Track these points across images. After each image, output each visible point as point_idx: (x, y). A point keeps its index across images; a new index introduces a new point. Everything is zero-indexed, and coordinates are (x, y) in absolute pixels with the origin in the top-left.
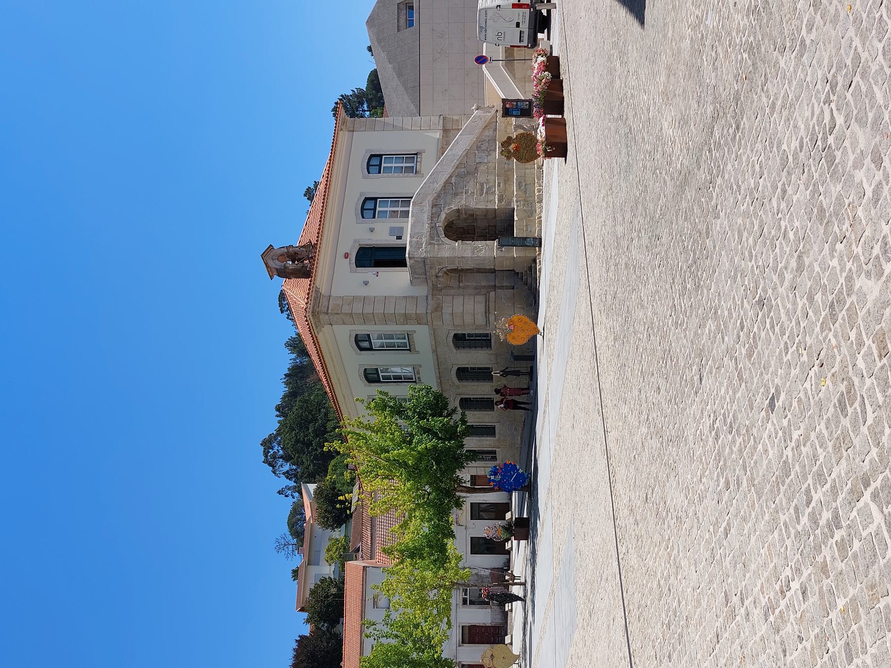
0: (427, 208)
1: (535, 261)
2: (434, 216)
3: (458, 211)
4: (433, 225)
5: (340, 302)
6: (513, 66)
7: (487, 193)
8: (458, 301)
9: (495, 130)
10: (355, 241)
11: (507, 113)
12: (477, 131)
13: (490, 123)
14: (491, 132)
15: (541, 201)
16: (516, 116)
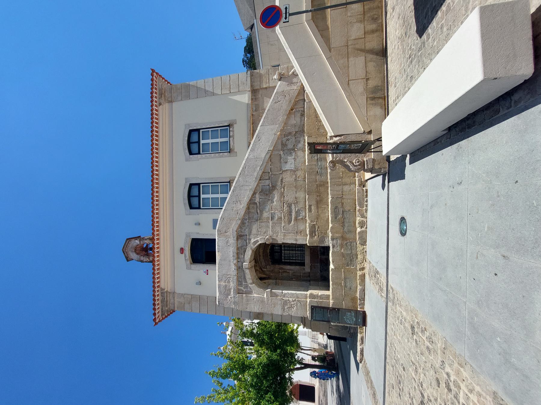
0: (232, 241)
2: (240, 252)
4: (240, 264)
5: (182, 300)
6: (325, 18)
7: (296, 219)
9: (303, 115)
10: (187, 235)
12: (281, 118)
13: (296, 103)
14: (298, 119)
15: (364, 242)
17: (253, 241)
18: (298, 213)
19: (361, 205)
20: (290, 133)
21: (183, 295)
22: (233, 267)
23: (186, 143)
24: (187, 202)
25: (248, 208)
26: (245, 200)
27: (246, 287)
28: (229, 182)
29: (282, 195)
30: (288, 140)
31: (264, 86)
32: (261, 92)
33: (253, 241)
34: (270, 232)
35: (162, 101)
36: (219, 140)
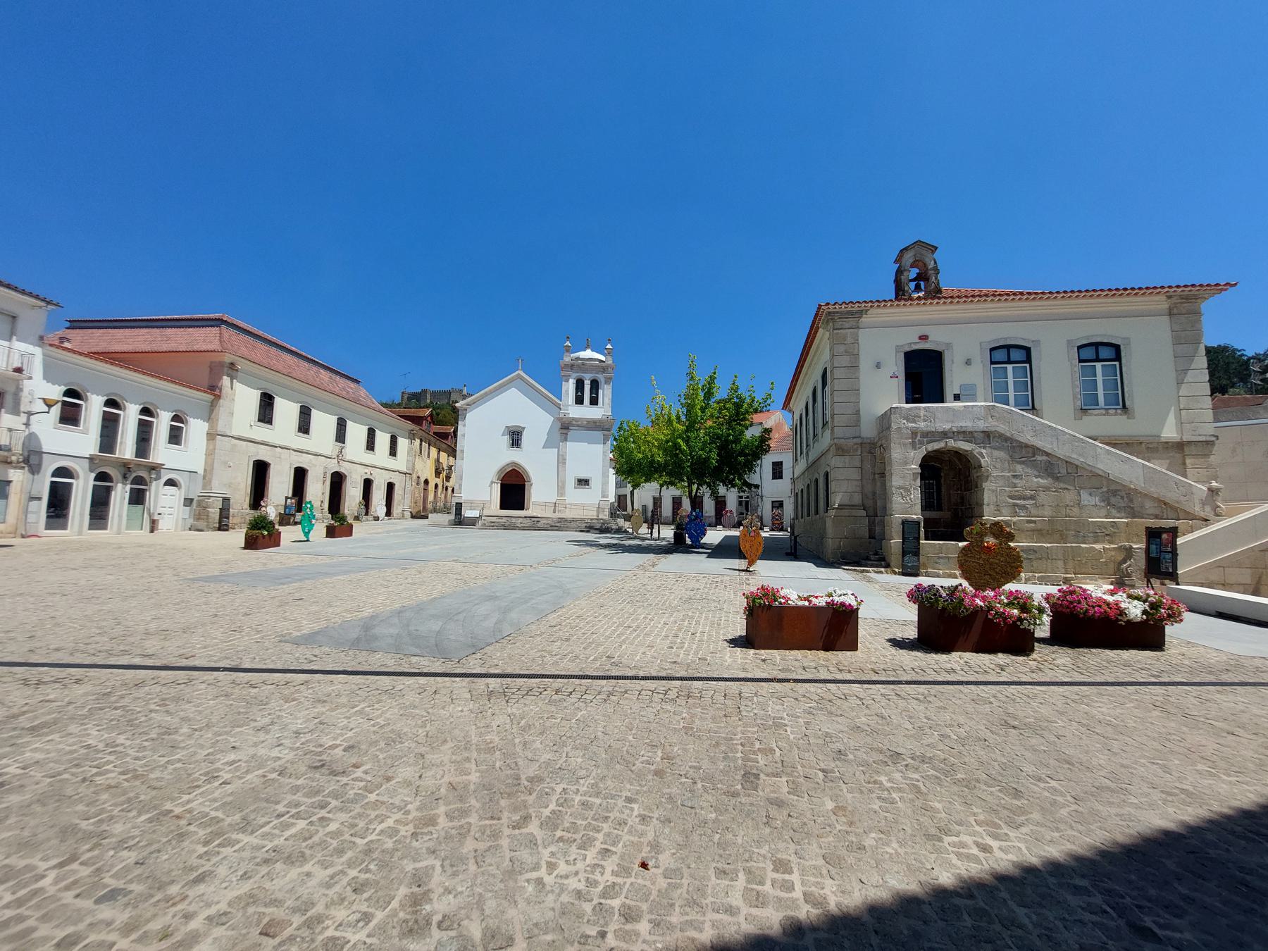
0: (981, 425)
1: (888, 566)
2: (968, 435)
3: (980, 466)
5: (849, 340)
8: (855, 474)
11: (1153, 534)
12: (1153, 490)
13: (1175, 509)
14: (1151, 511)
16: (1148, 550)
17: (984, 451)
18: (1024, 507)
19: (1041, 579)
20: (1131, 501)
21: (856, 341)
22: (947, 426)
23: (1099, 340)
24: (1002, 343)
25: (1027, 446)
26: (1038, 443)
27: (921, 443)
28: (1033, 408)
29: (1046, 489)
30: (1122, 498)
31: (1188, 461)
32: (1178, 456)
33: (984, 451)
34: (995, 473)
35: (1174, 300)
36: (1101, 392)
